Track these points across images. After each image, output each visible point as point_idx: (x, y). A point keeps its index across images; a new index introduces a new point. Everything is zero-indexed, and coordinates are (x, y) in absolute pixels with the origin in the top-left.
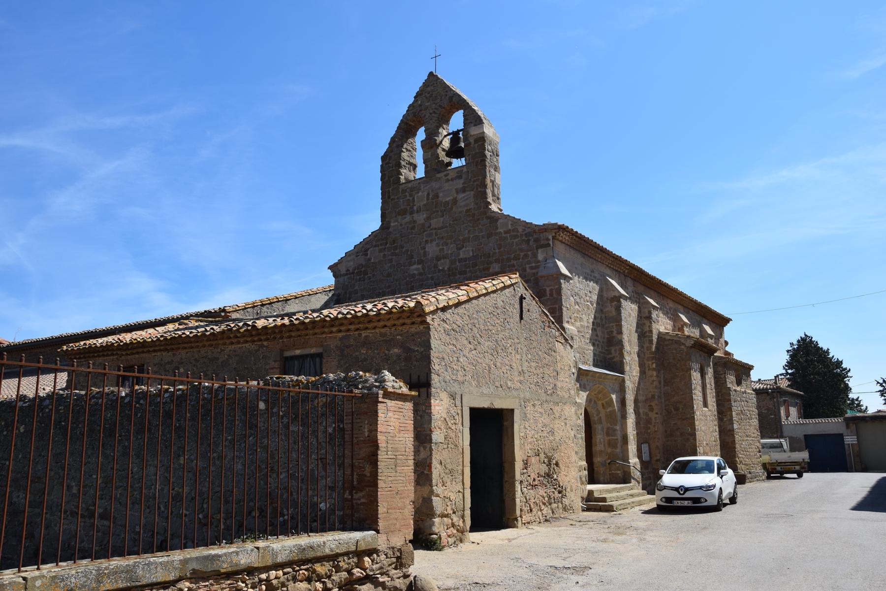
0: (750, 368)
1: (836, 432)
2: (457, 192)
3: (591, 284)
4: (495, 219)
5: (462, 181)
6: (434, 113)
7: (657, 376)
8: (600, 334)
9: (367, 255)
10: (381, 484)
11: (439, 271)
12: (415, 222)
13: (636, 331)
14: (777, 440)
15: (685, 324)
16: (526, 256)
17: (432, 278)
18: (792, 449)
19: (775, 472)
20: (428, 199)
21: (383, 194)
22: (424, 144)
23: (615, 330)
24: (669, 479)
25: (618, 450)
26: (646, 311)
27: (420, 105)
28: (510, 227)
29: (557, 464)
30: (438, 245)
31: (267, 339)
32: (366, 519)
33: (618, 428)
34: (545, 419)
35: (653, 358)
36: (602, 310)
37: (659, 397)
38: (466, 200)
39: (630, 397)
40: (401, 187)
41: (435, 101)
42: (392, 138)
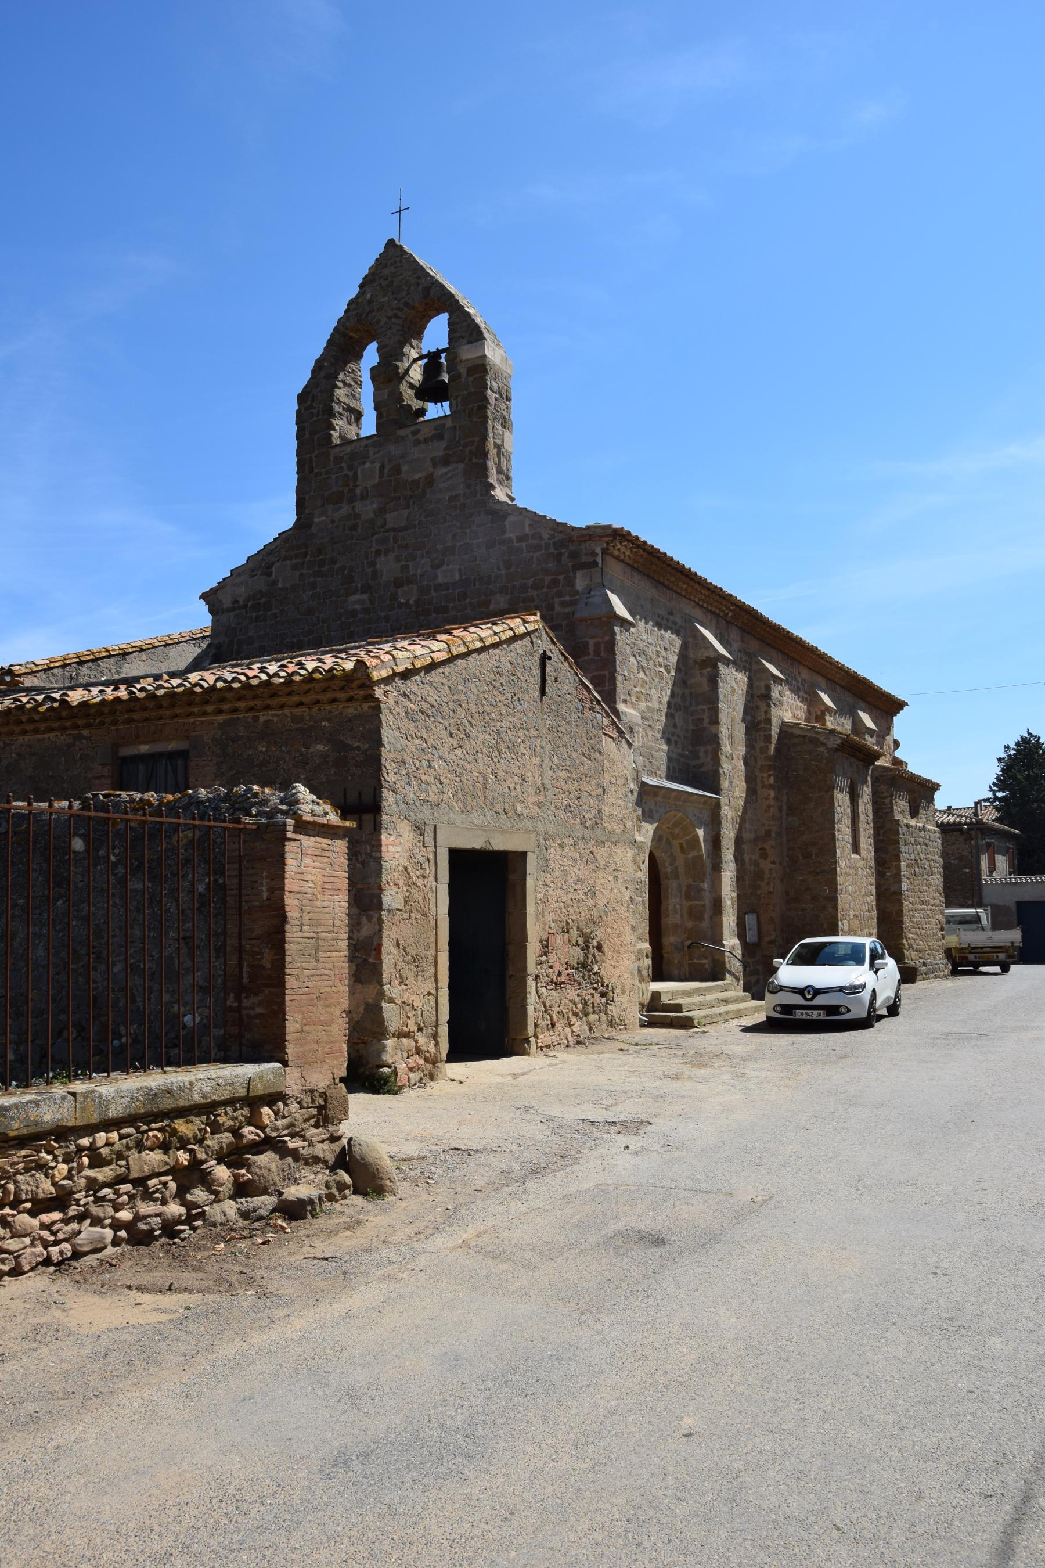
3: (668, 635)
5: (443, 444)
7: (776, 798)
9: (269, 574)
11: (400, 605)
12: (357, 516)
13: (743, 720)
15: (828, 709)
18: (996, 926)
19: (964, 963)
20: (381, 475)
21: (300, 464)
24: (790, 974)
25: (705, 924)
26: (762, 684)
27: (370, 302)
28: (527, 529)
29: (599, 947)
30: (398, 559)
31: (88, 726)
33: (706, 886)
37: (779, 834)
39: (728, 834)
40: (333, 452)
41: (396, 295)
42: (317, 362)
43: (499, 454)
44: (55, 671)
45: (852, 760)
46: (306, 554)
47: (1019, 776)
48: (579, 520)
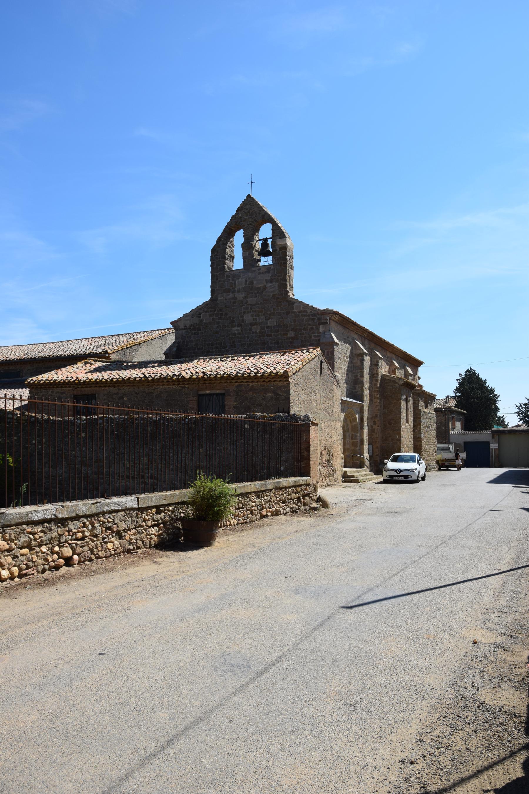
0: (436, 395)
1: (485, 441)
2: (267, 281)
3: (347, 345)
4: (293, 302)
6: (251, 224)
7: (380, 403)
8: (350, 376)
9: (200, 317)
10: (311, 459)
11: (253, 333)
12: (236, 298)
13: (369, 374)
14: (447, 445)
15: (397, 368)
16: (312, 328)
17: (248, 337)
19: (444, 466)
20: (246, 284)
22: (244, 246)
23: (359, 374)
24: (391, 465)
25: (358, 448)
26: (375, 360)
27: (241, 218)
28: (302, 309)
29: (332, 455)
30: (252, 316)
31: (188, 384)
32: (306, 473)
33: (358, 435)
34: (328, 430)
35: (378, 391)
36: (351, 362)
37: (380, 416)
38: (273, 288)
39: (366, 416)
40: (226, 273)
41: (250, 215)
42: (219, 238)
43: (290, 279)
44: (120, 352)
45: (407, 388)
46: (215, 311)
47: (466, 387)
48: (321, 306)
